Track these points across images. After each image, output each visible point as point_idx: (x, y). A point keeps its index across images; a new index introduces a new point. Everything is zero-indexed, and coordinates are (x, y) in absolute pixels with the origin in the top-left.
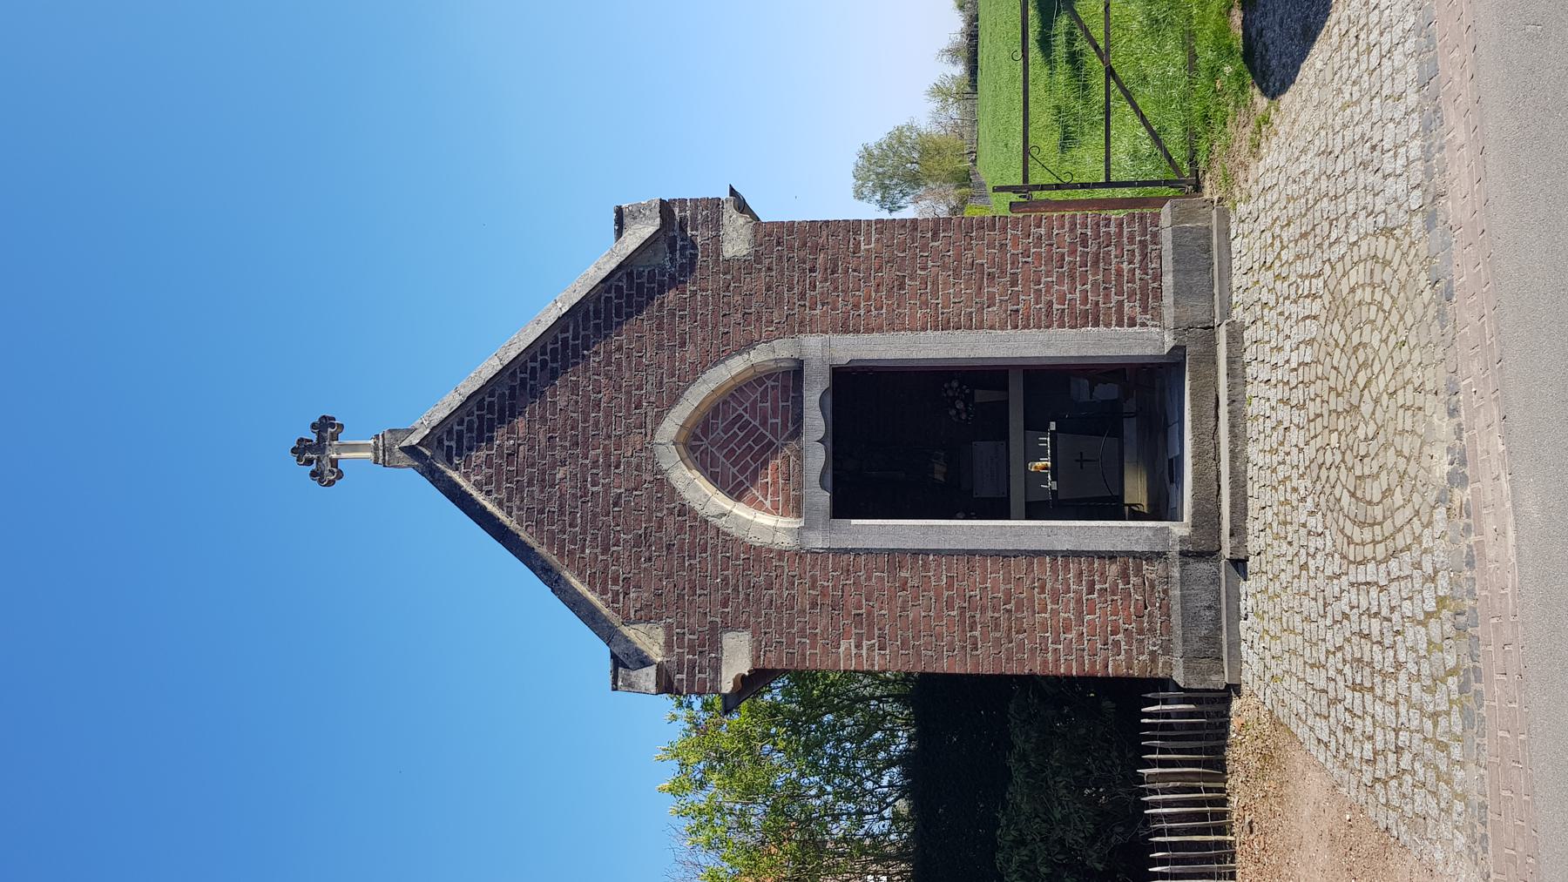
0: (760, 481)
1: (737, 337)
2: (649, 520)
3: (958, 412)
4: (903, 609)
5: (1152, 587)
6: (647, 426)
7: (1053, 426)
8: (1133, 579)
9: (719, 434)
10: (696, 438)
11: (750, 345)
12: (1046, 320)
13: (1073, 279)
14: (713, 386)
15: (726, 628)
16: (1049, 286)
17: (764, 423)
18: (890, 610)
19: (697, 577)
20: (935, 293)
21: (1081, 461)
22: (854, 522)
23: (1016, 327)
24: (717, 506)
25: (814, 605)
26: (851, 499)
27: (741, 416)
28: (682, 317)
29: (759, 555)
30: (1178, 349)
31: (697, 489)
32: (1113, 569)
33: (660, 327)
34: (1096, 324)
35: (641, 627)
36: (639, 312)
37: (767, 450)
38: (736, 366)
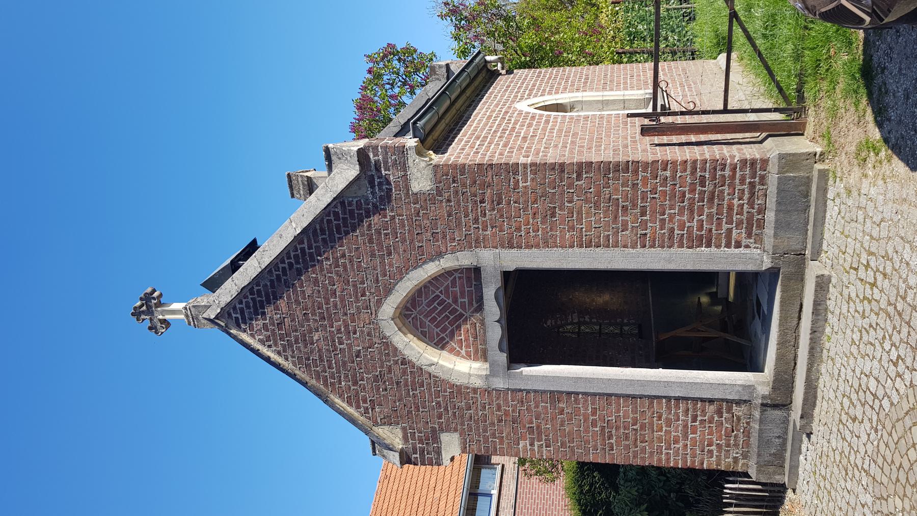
0: (456, 338)
2: (382, 367)
5: (739, 419)
9: (424, 306)
11: (440, 255)
12: (669, 241)
13: (692, 211)
15: (442, 430)
16: (671, 217)
17: (455, 301)
20: (580, 220)
23: (644, 246)
28: (386, 235)
31: (413, 349)
33: (371, 241)
34: (709, 245)
36: (354, 230)
37: (458, 320)
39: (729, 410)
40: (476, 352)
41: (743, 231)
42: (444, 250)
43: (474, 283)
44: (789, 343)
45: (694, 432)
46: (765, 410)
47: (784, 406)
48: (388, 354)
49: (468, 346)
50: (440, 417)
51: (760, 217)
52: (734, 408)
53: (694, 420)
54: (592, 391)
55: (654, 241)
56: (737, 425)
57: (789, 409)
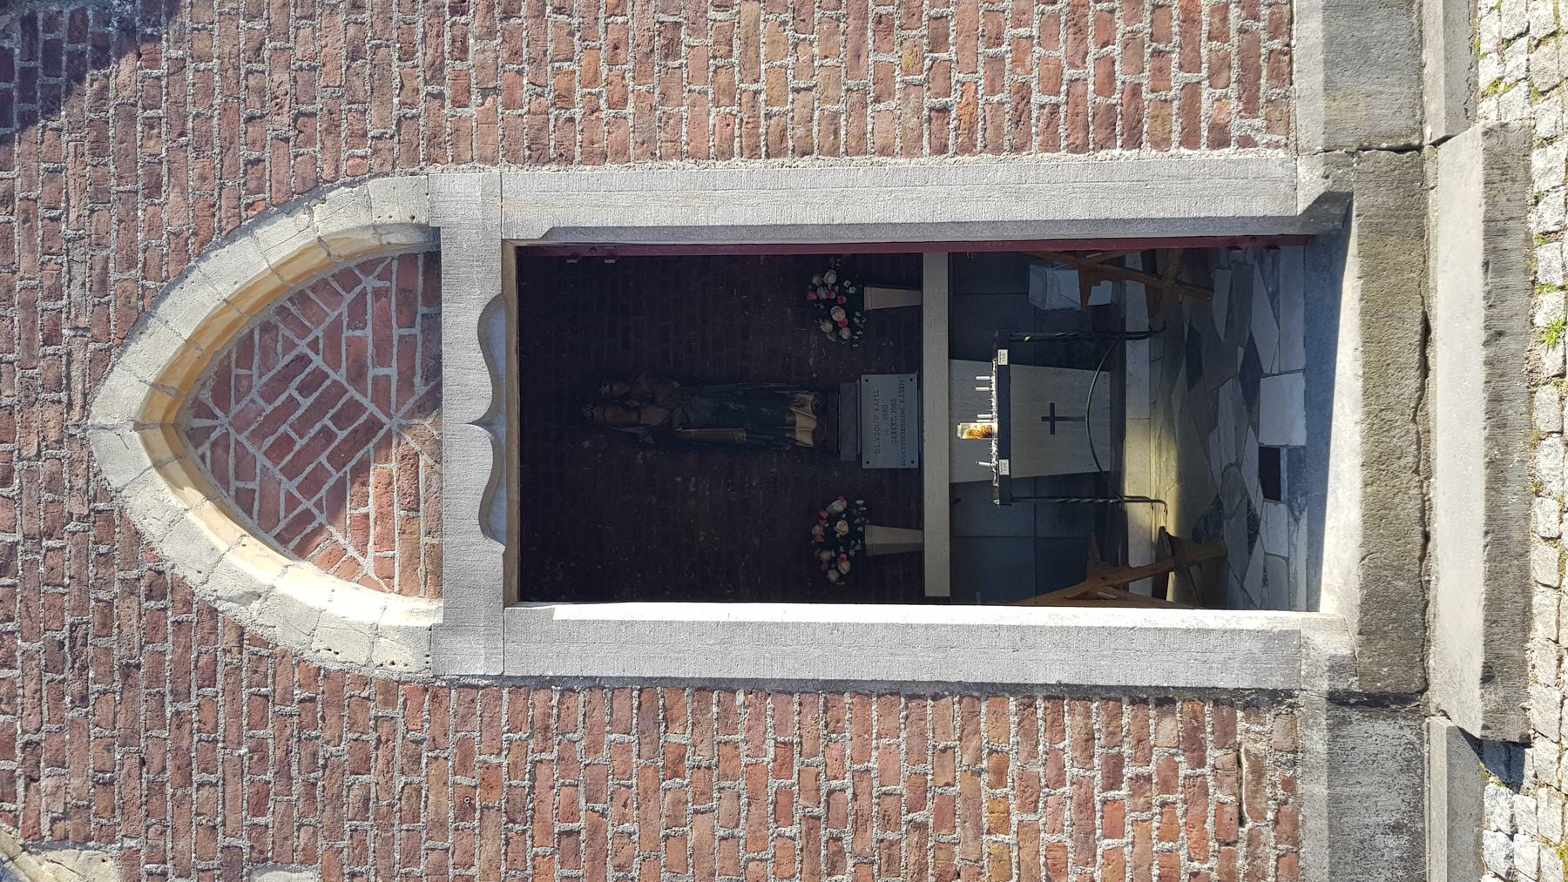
0: (351, 511)
1: (282, 170)
2: (81, 608)
3: (837, 327)
4: (675, 819)
5: (1258, 771)
6: (71, 391)
7: (1003, 357)
8: (1213, 755)
9: (252, 403)
10: (201, 410)
11: (313, 190)
12: (1016, 131)
13: (1079, 30)
14: (226, 290)
16: (1021, 47)
17: (357, 376)
18: (643, 822)
19: (191, 741)
20: (750, 66)
21: (1052, 419)
22: (565, 611)
23: (942, 150)
24: (237, 574)
25: (465, 810)
26: (562, 552)
27: (303, 360)
28: (150, 124)
29: (337, 691)
30: (1335, 205)
31: (193, 536)
32: (1166, 730)
33: (99, 147)
34: (1133, 141)
35: (67, 856)
36: (51, 110)
37: (365, 438)
38: (277, 245)
39: (1225, 734)
40: (412, 559)
41: (1233, 90)
42: (328, 172)
43: (422, 309)
44: (1402, 460)
45: (1114, 831)
46: (1344, 722)
47: (1403, 699)
48: (106, 559)
49: (385, 540)
50: (258, 808)
51: (1277, 44)
52: (1241, 726)
53: (1113, 781)
54: (778, 674)
55: (971, 130)
56: (1255, 792)
57: (1421, 714)
